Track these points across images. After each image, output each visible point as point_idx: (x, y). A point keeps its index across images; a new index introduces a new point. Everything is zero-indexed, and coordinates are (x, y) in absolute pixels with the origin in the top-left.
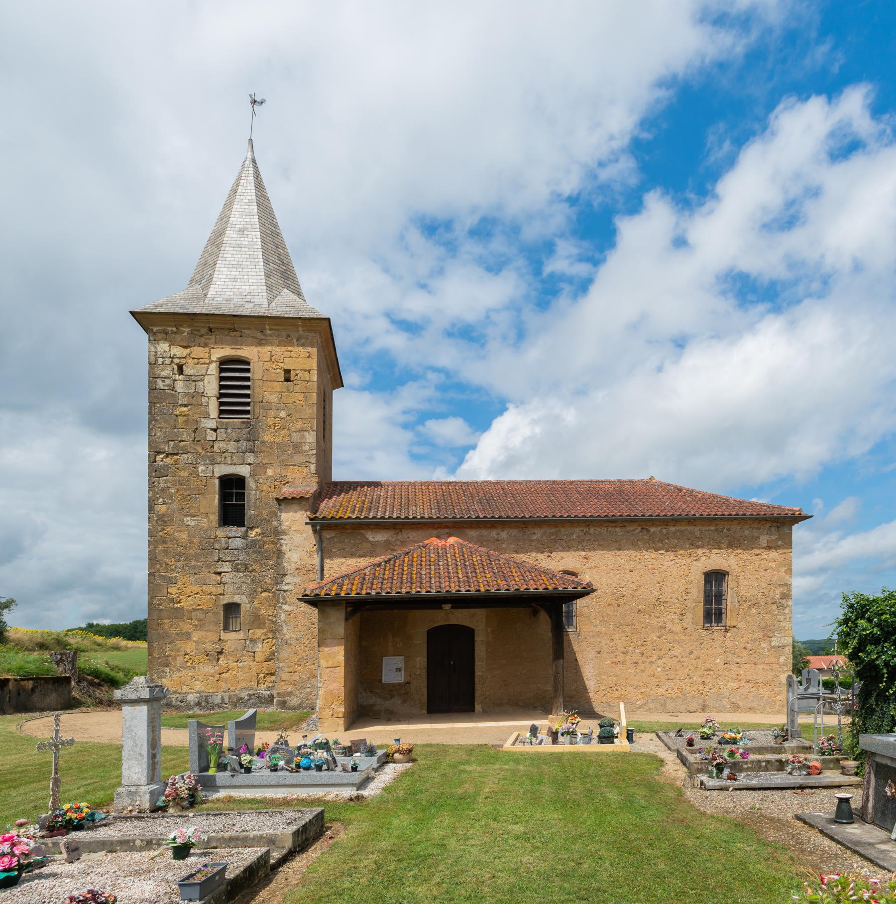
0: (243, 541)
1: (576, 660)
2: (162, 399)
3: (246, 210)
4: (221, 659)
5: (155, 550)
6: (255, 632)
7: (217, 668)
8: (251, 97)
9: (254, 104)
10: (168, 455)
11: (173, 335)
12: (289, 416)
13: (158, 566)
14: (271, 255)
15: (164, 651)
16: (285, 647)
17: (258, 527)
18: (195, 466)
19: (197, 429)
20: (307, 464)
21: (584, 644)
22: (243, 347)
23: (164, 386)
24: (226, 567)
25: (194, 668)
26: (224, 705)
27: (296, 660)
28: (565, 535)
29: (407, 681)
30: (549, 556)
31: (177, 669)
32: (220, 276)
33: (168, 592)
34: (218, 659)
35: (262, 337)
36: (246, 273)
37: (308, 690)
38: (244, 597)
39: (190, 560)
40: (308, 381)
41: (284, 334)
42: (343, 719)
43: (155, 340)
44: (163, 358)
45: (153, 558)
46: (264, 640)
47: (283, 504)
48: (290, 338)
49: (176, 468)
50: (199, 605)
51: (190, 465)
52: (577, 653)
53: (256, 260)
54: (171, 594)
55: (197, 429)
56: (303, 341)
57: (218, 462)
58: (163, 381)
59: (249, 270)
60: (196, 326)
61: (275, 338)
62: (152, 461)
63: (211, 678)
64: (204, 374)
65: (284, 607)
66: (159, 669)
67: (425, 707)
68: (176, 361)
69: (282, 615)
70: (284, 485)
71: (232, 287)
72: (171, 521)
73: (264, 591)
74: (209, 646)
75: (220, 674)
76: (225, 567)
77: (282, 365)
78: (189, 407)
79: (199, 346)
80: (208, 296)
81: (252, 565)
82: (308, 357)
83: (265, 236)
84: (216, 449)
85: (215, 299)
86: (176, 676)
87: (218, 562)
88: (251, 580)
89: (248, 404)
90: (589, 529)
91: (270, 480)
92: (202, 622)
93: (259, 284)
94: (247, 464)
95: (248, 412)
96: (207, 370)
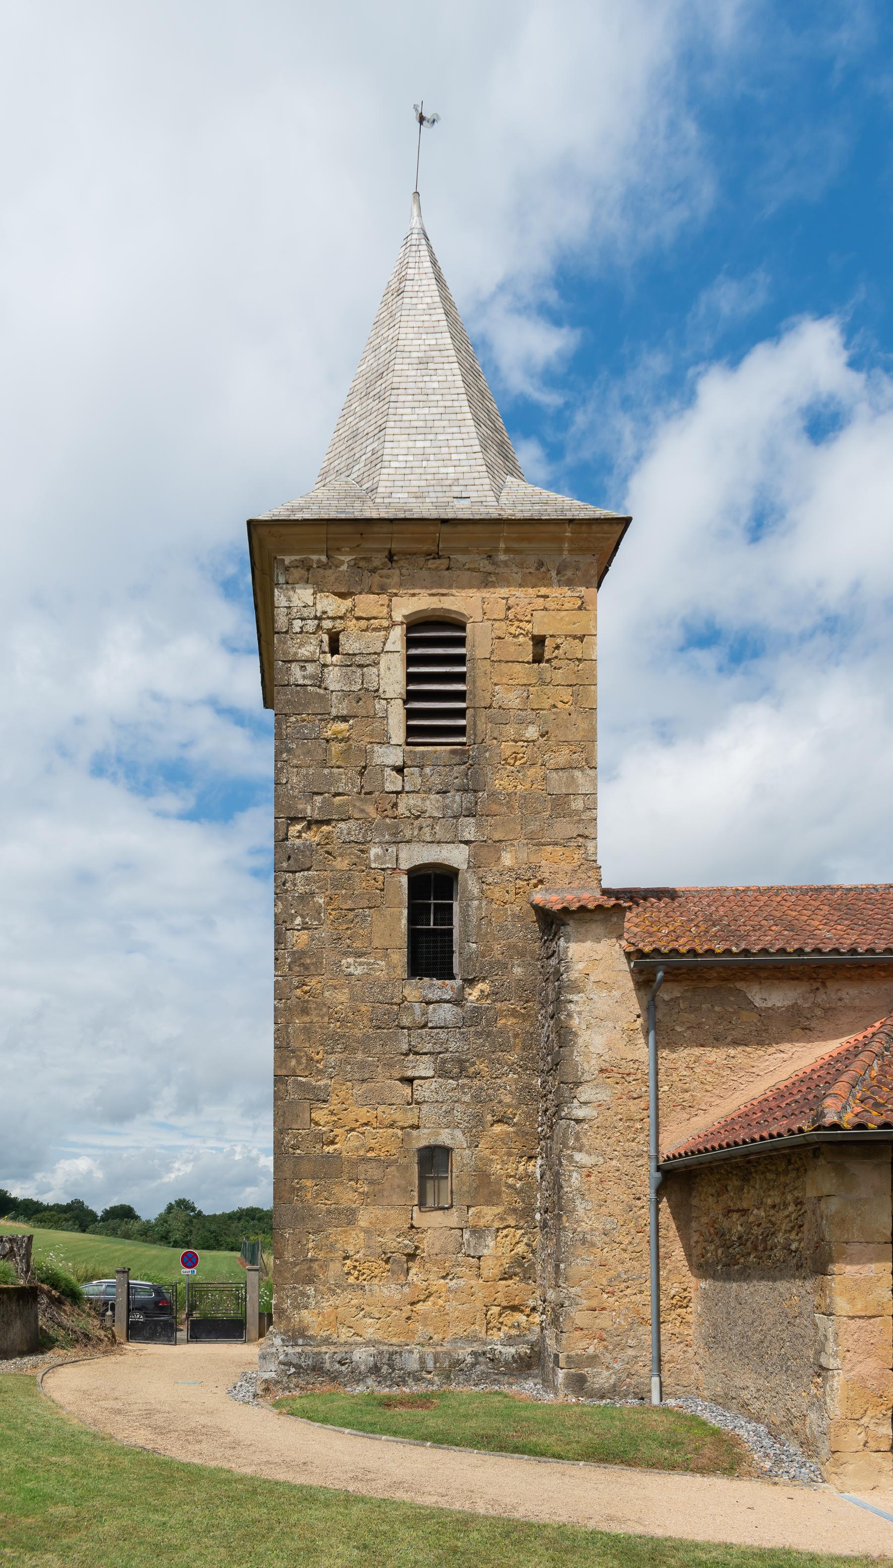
0: (455, 1008)
2: (301, 705)
3: (426, 324)
4: (413, 1271)
5: (287, 1027)
6: (480, 1212)
7: (406, 1290)
8: (416, 110)
11: (321, 571)
12: (542, 736)
13: (293, 1062)
15: (304, 1250)
16: (581, 1250)
19: (365, 768)
20: (580, 840)
22: (454, 591)
23: (304, 677)
24: (424, 1067)
25: (363, 1288)
27: (605, 1283)
31: (329, 1289)
32: (396, 451)
34: (408, 1269)
35: (490, 568)
36: (445, 443)
37: (631, 1352)
38: (458, 1133)
39: (354, 1051)
40: (579, 660)
41: (532, 560)
43: (287, 583)
44: (303, 619)
45: (284, 1044)
46: (498, 1230)
47: (571, 922)
50: (371, 1149)
51: (353, 844)
53: (460, 417)
54: (317, 1124)
55: (365, 768)
56: (569, 573)
57: (407, 838)
58: (303, 668)
59: (449, 437)
61: (515, 569)
62: (281, 840)
63: (395, 1312)
64: (379, 650)
65: (578, 1157)
66: (295, 1288)
68: (327, 624)
69: (575, 1174)
70: (535, 886)
71: (421, 471)
72: (318, 964)
73: (499, 1121)
74: (391, 1241)
75: (413, 1304)
76: (422, 1066)
77: (529, 627)
78: (351, 722)
80: (379, 490)
81: (474, 1064)
84: (402, 810)
85: (394, 495)
87: (407, 1055)
88: (472, 1096)
89: (461, 714)
91: (506, 877)
92: (377, 1188)
93: (472, 462)
94: (461, 842)
95: (460, 731)
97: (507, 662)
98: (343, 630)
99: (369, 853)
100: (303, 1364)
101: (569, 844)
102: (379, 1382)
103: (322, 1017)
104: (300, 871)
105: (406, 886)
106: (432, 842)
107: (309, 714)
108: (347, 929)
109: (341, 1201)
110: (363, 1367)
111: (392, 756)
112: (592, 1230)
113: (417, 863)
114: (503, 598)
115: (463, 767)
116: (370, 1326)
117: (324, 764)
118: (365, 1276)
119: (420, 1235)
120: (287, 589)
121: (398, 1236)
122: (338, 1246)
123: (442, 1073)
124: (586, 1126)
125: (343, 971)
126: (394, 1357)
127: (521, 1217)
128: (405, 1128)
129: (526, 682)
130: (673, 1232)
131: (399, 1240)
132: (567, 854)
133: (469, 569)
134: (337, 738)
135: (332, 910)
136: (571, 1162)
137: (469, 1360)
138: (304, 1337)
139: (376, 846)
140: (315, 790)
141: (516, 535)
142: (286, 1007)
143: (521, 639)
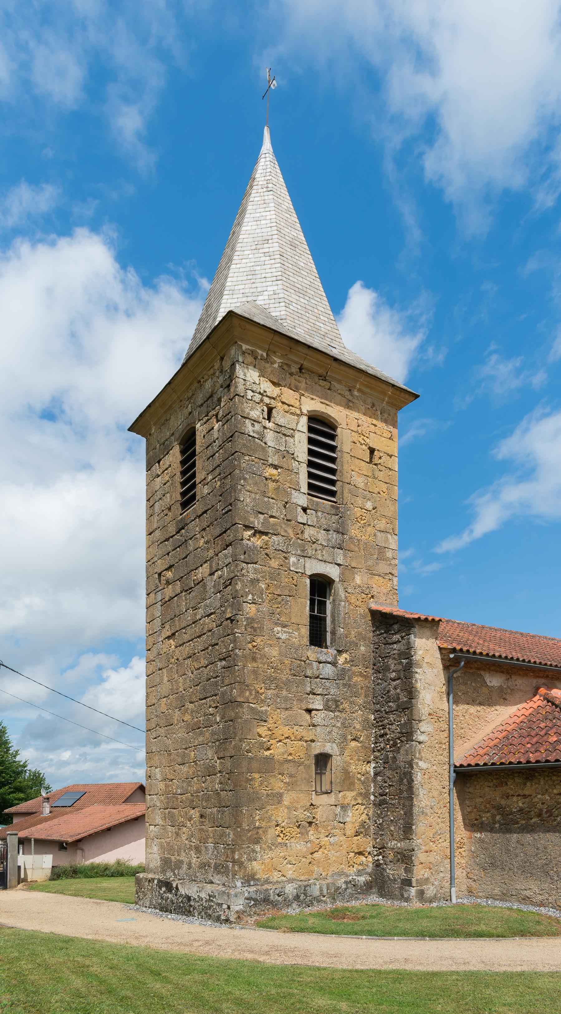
0: (333, 668)
2: (251, 449)
5: (243, 669)
7: (309, 845)
13: (247, 693)
15: (254, 822)
16: (422, 818)
22: (332, 405)
24: (317, 703)
25: (286, 845)
27: (431, 836)
31: (268, 846)
35: (350, 398)
38: (335, 746)
41: (369, 401)
43: (243, 363)
44: (253, 391)
45: (242, 680)
47: (417, 626)
50: (291, 754)
51: (280, 552)
54: (260, 736)
56: (386, 415)
57: (309, 555)
61: (362, 403)
65: (421, 763)
66: (249, 847)
68: (267, 400)
69: (419, 774)
72: (261, 628)
73: (354, 739)
76: (317, 702)
78: (279, 470)
84: (306, 536)
87: (309, 694)
94: (336, 564)
95: (333, 494)
97: (358, 458)
98: (275, 408)
99: (289, 560)
100: (258, 898)
101: (385, 577)
102: (299, 905)
103: (264, 664)
104: (251, 564)
105: (309, 586)
106: (322, 561)
107: (256, 458)
108: (278, 607)
109: (275, 788)
110: (291, 897)
111: (301, 500)
112: (426, 806)
113: (315, 572)
114: (356, 419)
115: (337, 517)
116: (290, 869)
117: (264, 494)
118: (287, 837)
119: (316, 810)
120: (243, 367)
121: (304, 811)
122: (273, 818)
123: (327, 708)
124: (423, 746)
125: (275, 635)
126: (307, 888)
127: (364, 798)
128: (308, 741)
129: (366, 474)
130: (457, 807)
131: (305, 813)
132: (385, 583)
133: (340, 394)
134: (271, 478)
135: (269, 593)
136: (417, 766)
137: (344, 886)
138: (254, 879)
139: (294, 556)
140: (260, 510)
141: (366, 383)
142: (243, 655)
143: (364, 447)
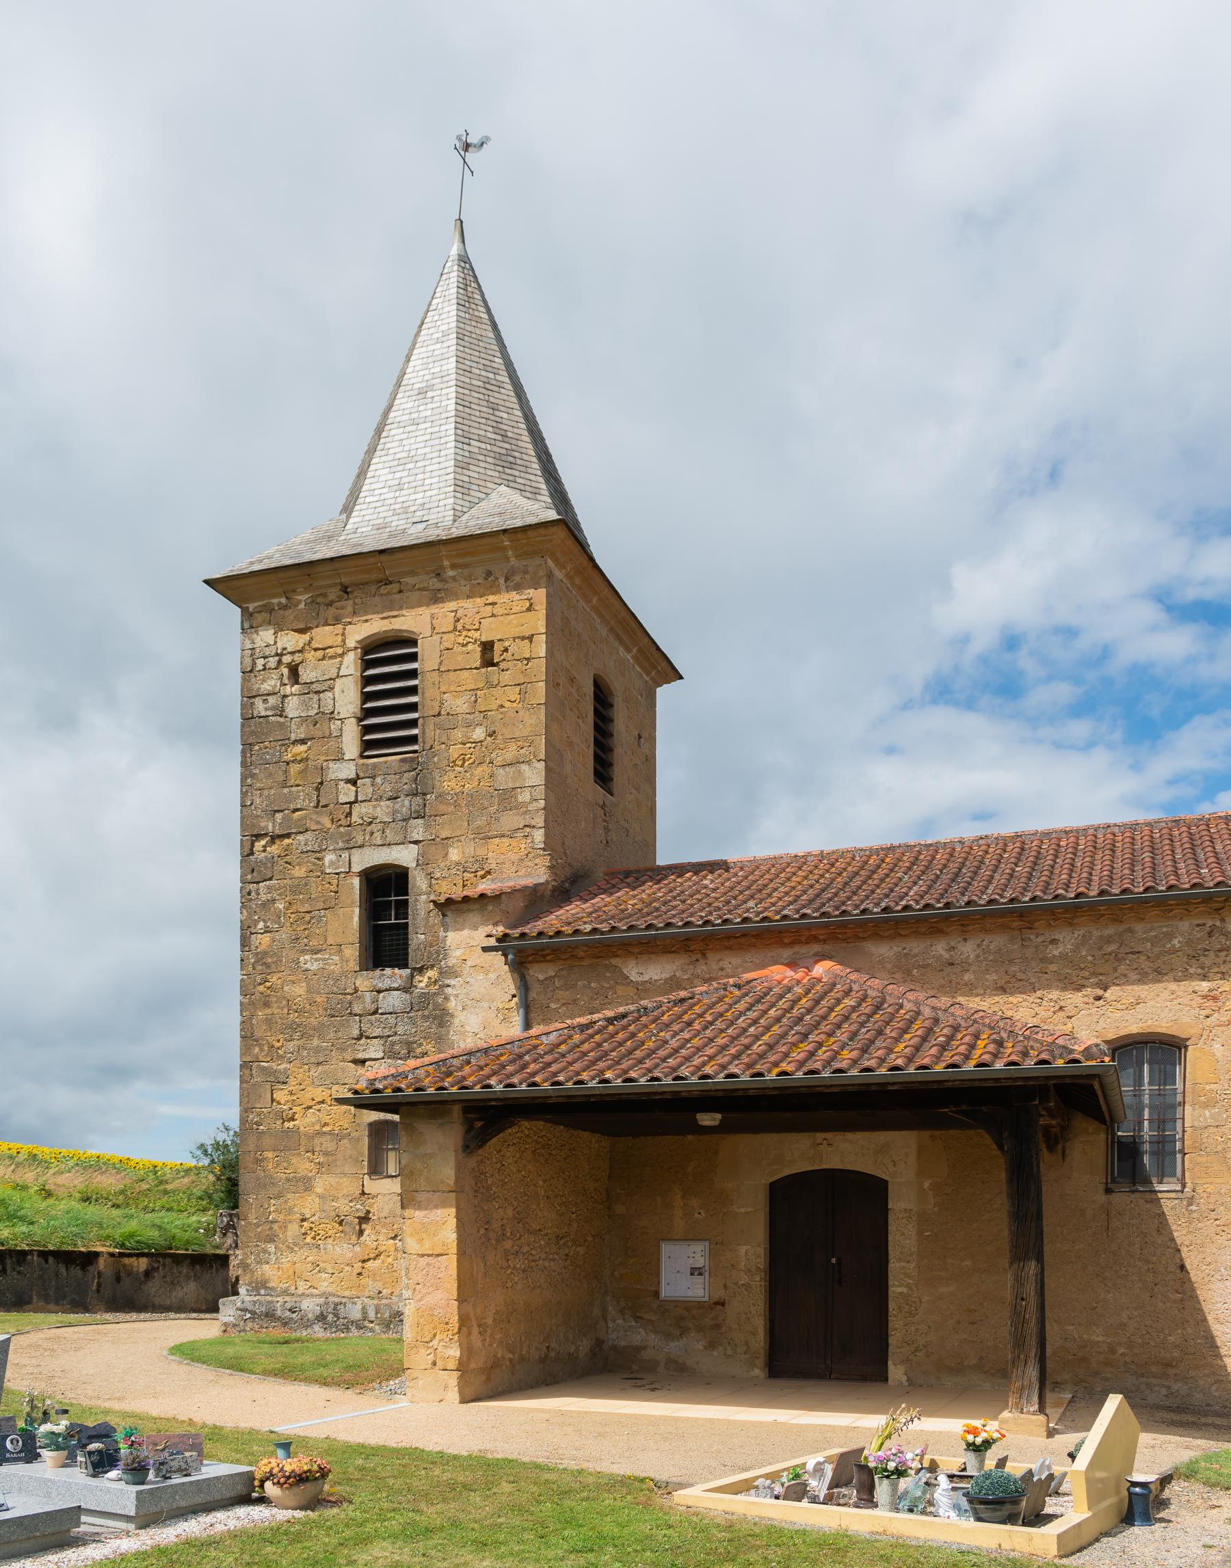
0: (404, 996)
1: (1182, 1267)
4: (366, 1233)
5: (251, 1019)
7: (357, 1249)
9: (466, 150)
10: (274, 838)
11: (282, 612)
12: (490, 736)
13: (257, 1050)
14: (476, 425)
17: (432, 967)
18: (318, 855)
19: (321, 783)
20: (528, 830)
21: (1208, 1226)
22: (404, 612)
23: (266, 709)
25: (318, 1247)
26: (366, 1324)
28: (1147, 940)
29: (716, 1297)
30: (1098, 998)
31: (288, 1247)
33: (273, 1100)
34: (361, 1232)
35: (439, 585)
39: (310, 1037)
40: (528, 659)
41: (480, 571)
42: (456, 1374)
44: (264, 658)
45: (249, 1034)
47: (449, 913)
48: (492, 578)
49: (286, 863)
50: (326, 1124)
51: (310, 854)
52: (1184, 1250)
54: (279, 1103)
55: (321, 783)
56: (517, 578)
57: (359, 843)
58: (265, 701)
60: (320, 587)
61: (463, 582)
66: (258, 1246)
67: (761, 1361)
68: (287, 659)
70: (483, 877)
74: (344, 1206)
75: (364, 1261)
76: (373, 1049)
77: (476, 635)
79: (326, 624)
81: (421, 1045)
82: (529, 609)
83: (467, 392)
84: (355, 818)
86: (286, 1259)
87: (359, 1039)
90: (1223, 920)
91: (454, 871)
92: (331, 1158)
94: (411, 842)
95: (413, 740)
96: (339, 668)
